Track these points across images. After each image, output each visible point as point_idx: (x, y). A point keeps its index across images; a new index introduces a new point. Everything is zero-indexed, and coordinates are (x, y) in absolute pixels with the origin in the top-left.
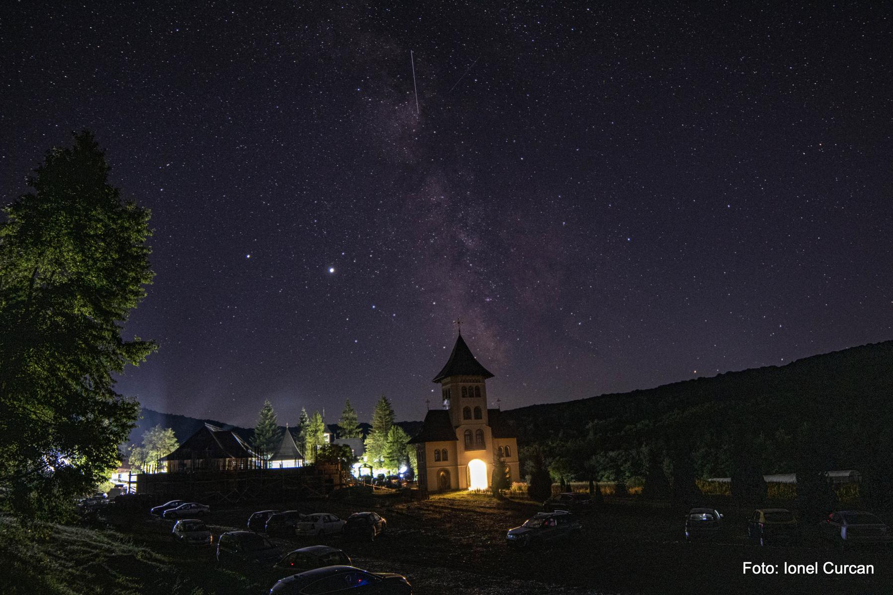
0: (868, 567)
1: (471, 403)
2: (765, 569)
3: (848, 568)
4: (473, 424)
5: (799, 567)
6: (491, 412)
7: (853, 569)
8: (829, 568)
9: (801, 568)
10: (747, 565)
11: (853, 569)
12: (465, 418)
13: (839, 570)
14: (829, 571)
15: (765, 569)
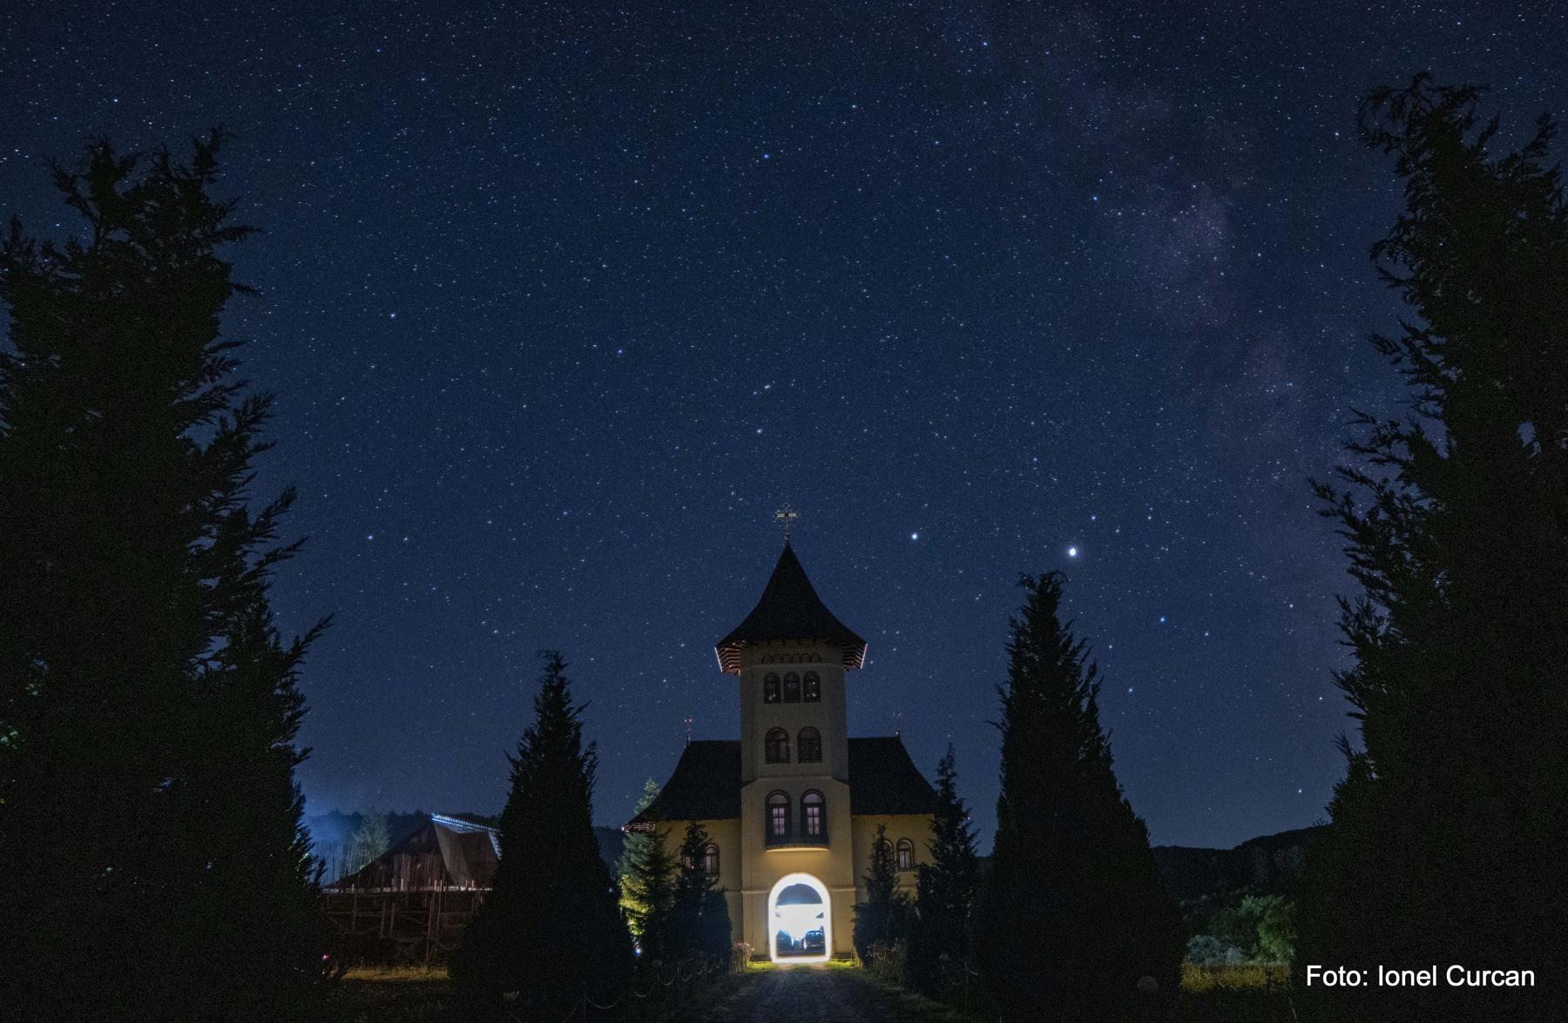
0: (1524, 973)
1: (792, 718)
2: (1343, 977)
3: (1489, 977)
6: (857, 747)
7: (1498, 978)
8: (1456, 975)
9: (1408, 976)
10: (1313, 971)
11: (1498, 978)
12: (768, 761)
13: (1473, 980)
15: (1343, 977)
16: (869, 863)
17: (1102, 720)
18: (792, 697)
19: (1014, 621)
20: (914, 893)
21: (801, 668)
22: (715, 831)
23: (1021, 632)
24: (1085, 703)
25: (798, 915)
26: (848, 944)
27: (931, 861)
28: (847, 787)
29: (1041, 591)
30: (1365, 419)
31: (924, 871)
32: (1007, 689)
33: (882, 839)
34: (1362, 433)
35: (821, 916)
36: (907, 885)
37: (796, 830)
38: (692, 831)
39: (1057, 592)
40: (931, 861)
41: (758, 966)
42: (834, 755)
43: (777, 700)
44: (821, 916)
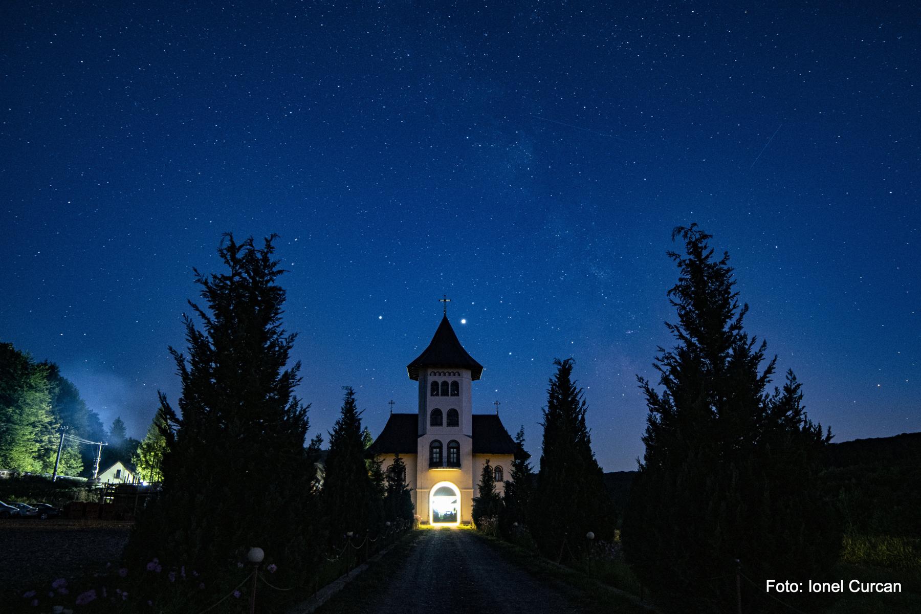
0: (895, 585)
1: (444, 404)
2: (788, 587)
3: (874, 587)
4: (444, 434)
5: (824, 585)
6: (477, 420)
7: (880, 588)
8: (855, 586)
9: (826, 586)
10: (770, 583)
11: (880, 588)
12: (432, 425)
13: (865, 589)
14: (855, 589)
15: (788, 587)
16: (481, 478)
17: (587, 424)
18: (445, 393)
19: (551, 380)
20: (502, 495)
21: (450, 380)
22: (406, 460)
23: (554, 384)
24: (580, 416)
25: (444, 501)
26: (469, 517)
27: (511, 480)
28: (471, 440)
29: (564, 367)
30: (662, 350)
31: (508, 484)
32: (547, 409)
33: (488, 467)
34: (661, 355)
35: (455, 502)
36: (499, 488)
37: (445, 460)
38: (397, 461)
39: (570, 368)
40: (511, 480)
41: (424, 527)
42: (466, 425)
43: (437, 395)
44: (455, 502)
